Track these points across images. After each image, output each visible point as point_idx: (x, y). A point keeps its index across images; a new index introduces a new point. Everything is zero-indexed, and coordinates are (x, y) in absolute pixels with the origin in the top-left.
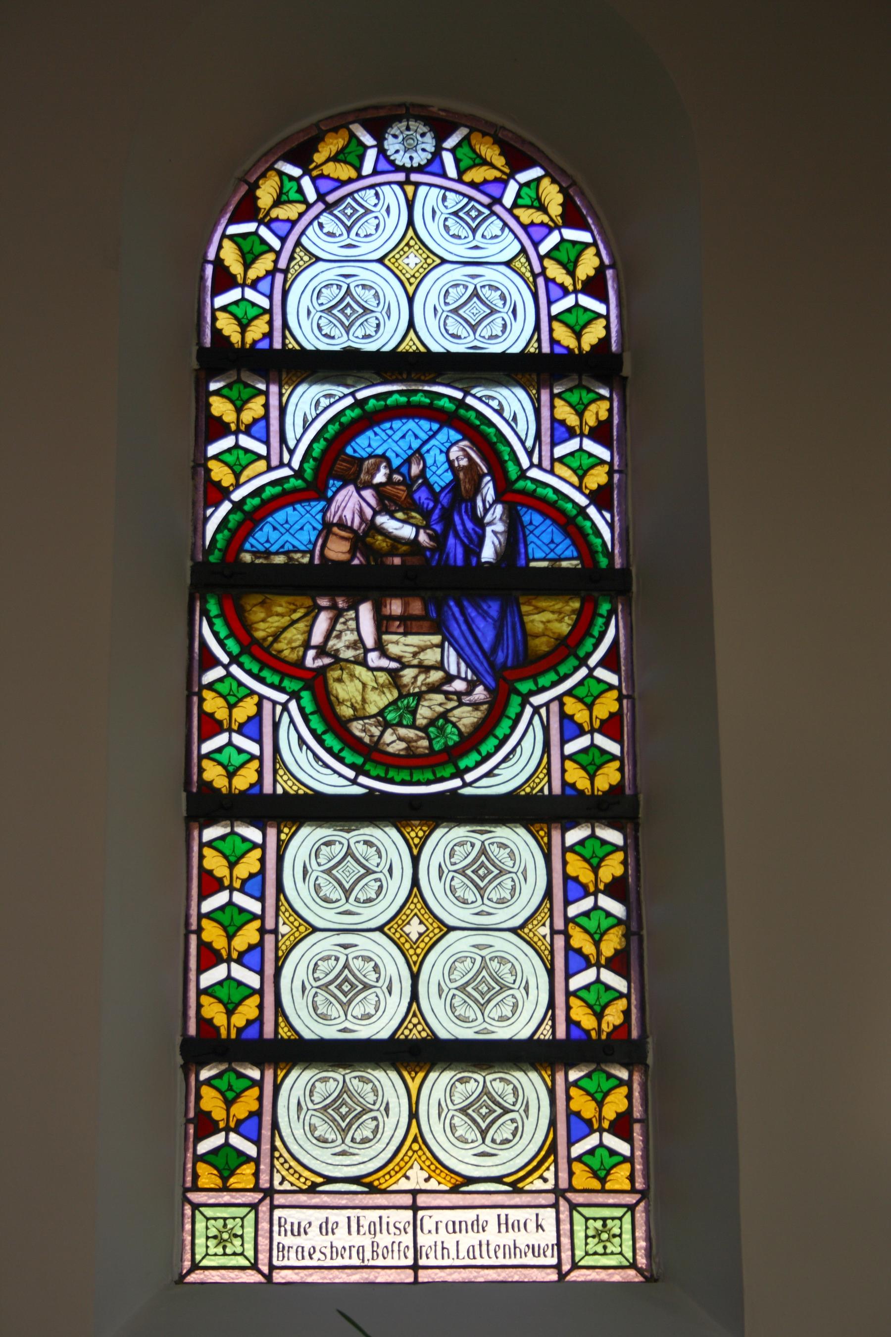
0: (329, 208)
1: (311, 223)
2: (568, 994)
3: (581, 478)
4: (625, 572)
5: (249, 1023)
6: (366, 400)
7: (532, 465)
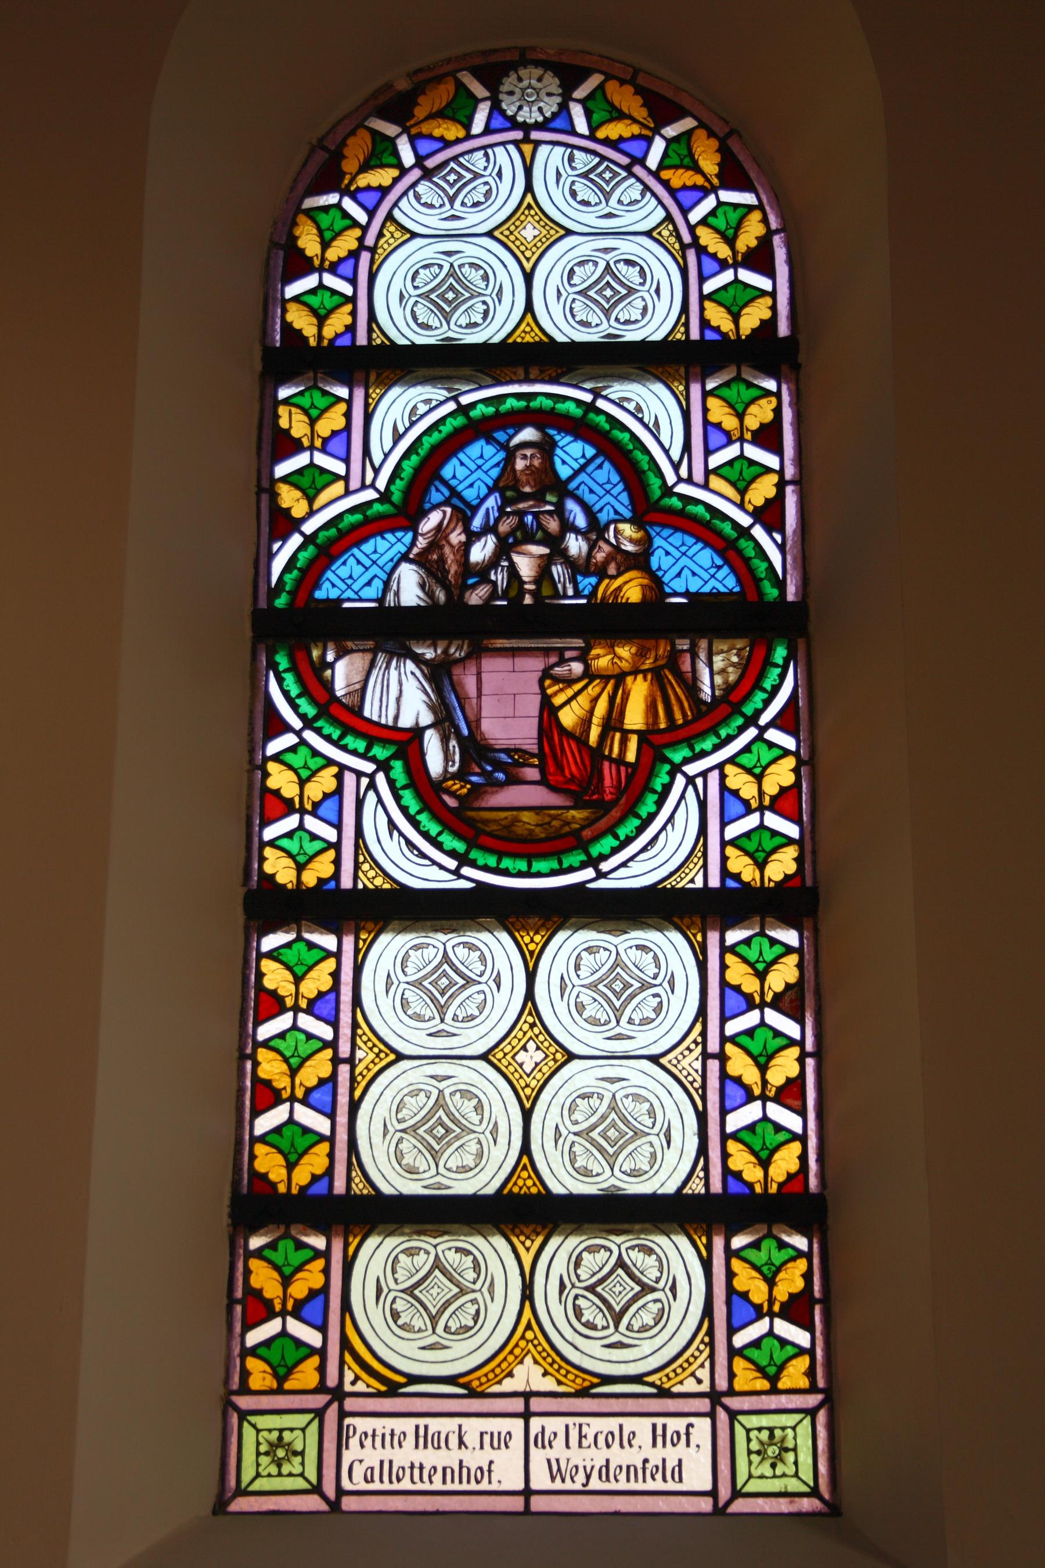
0: (428, 174)
1: (405, 193)
2: (725, 1137)
3: (742, 493)
4: (801, 606)
5: (315, 1178)
6: (473, 405)
7: (680, 480)
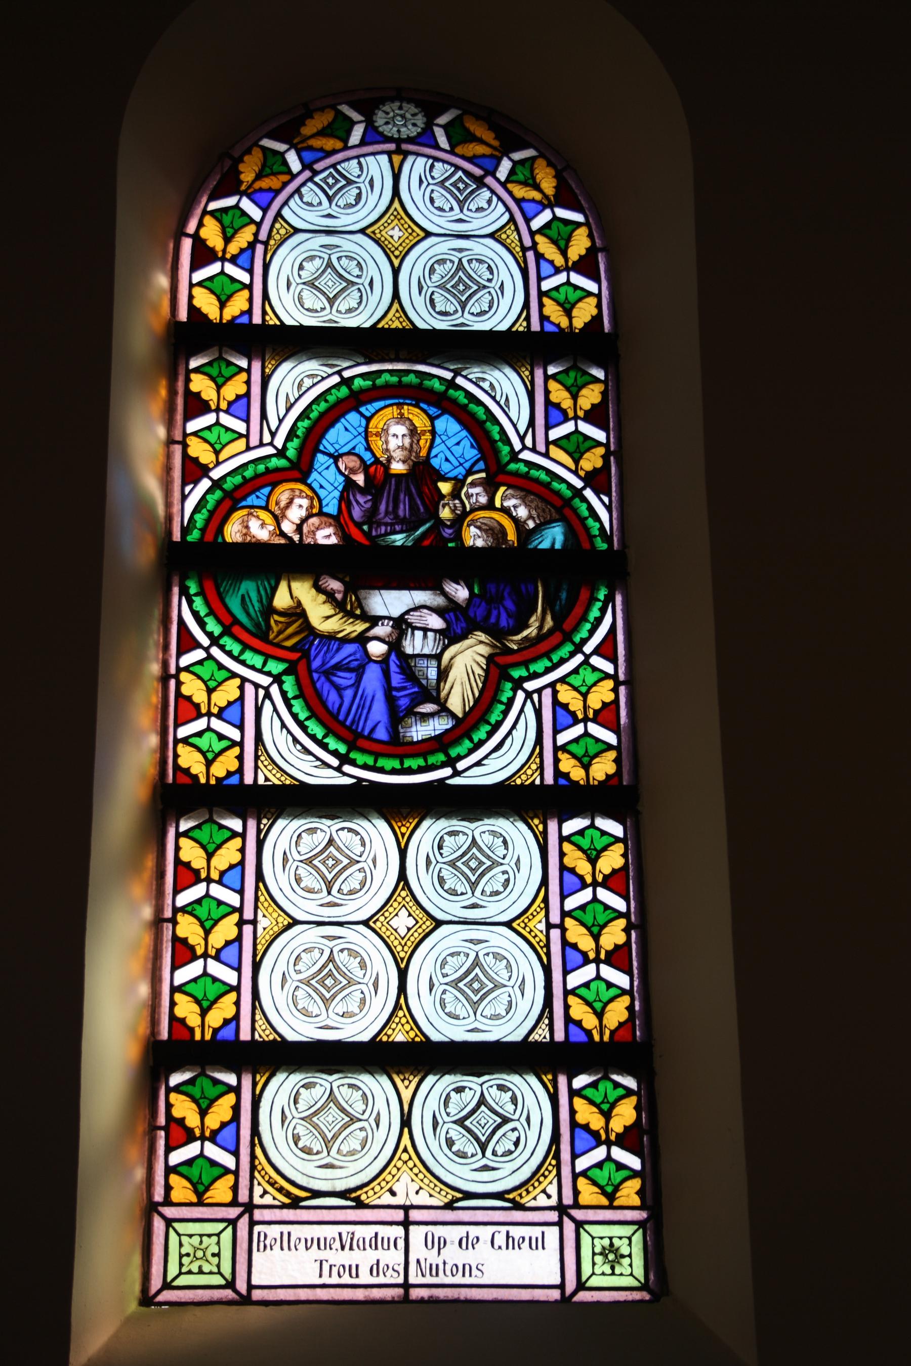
2: (567, 993)
5: (226, 1022)
7: (524, 447)
